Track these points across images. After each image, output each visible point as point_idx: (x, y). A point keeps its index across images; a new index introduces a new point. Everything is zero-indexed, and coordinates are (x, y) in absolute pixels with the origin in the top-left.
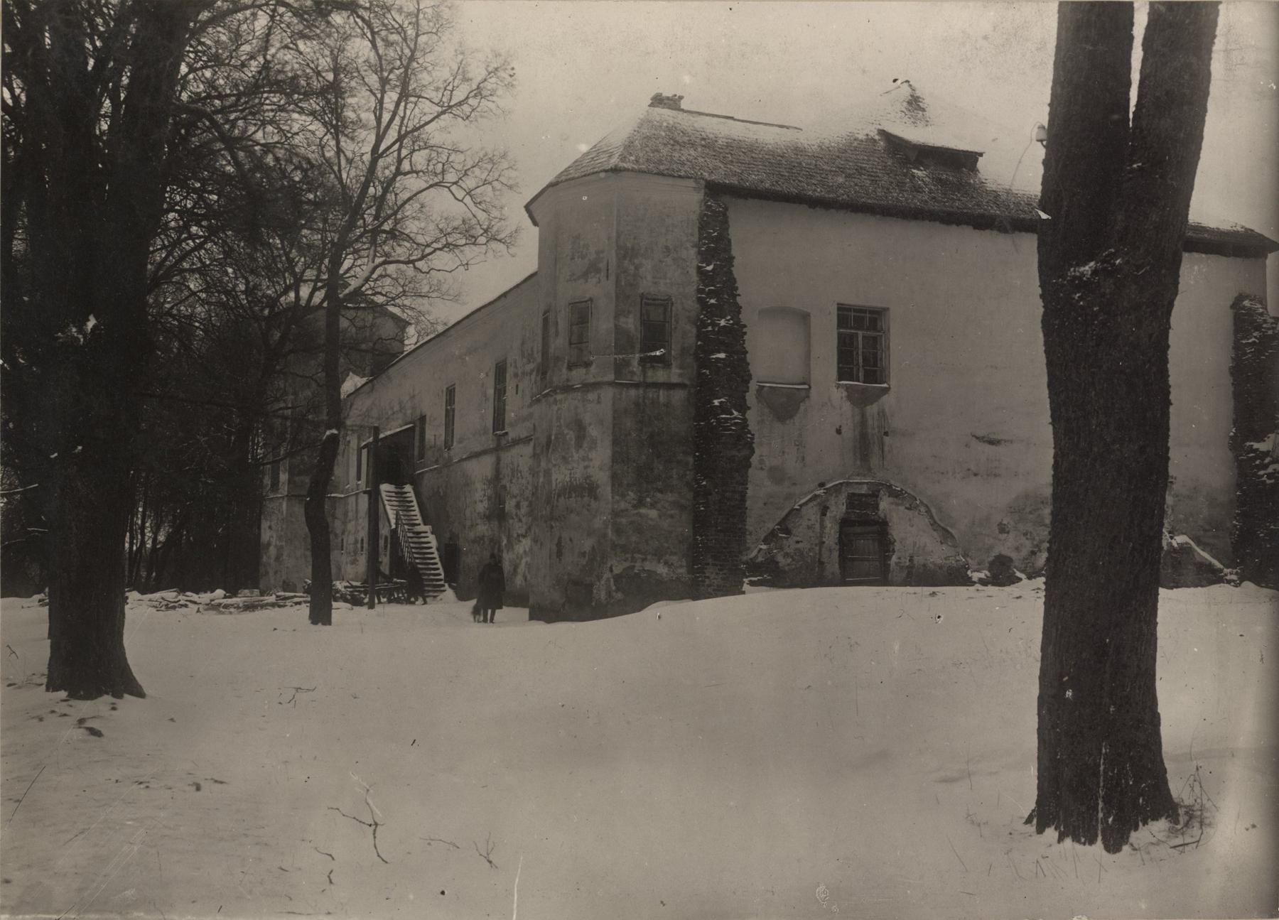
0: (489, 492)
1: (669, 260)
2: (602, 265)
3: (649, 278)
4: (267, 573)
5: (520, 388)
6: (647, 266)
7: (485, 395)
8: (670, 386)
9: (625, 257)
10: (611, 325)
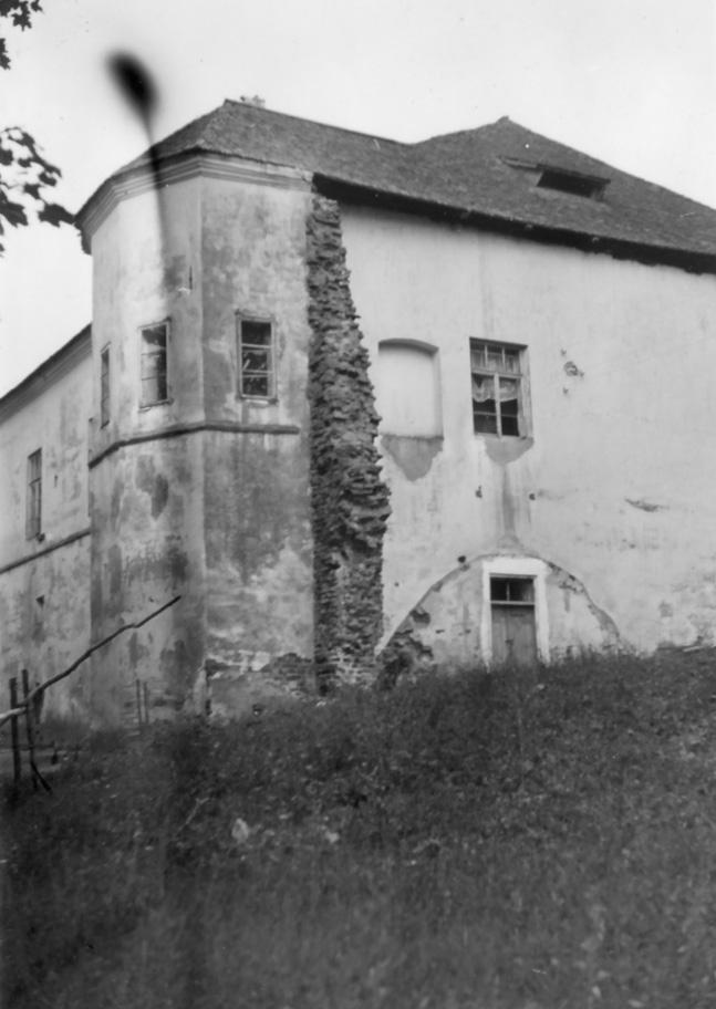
0: (21, 609)
1: (270, 271)
3: (246, 289)
5: (60, 479)
6: (243, 277)
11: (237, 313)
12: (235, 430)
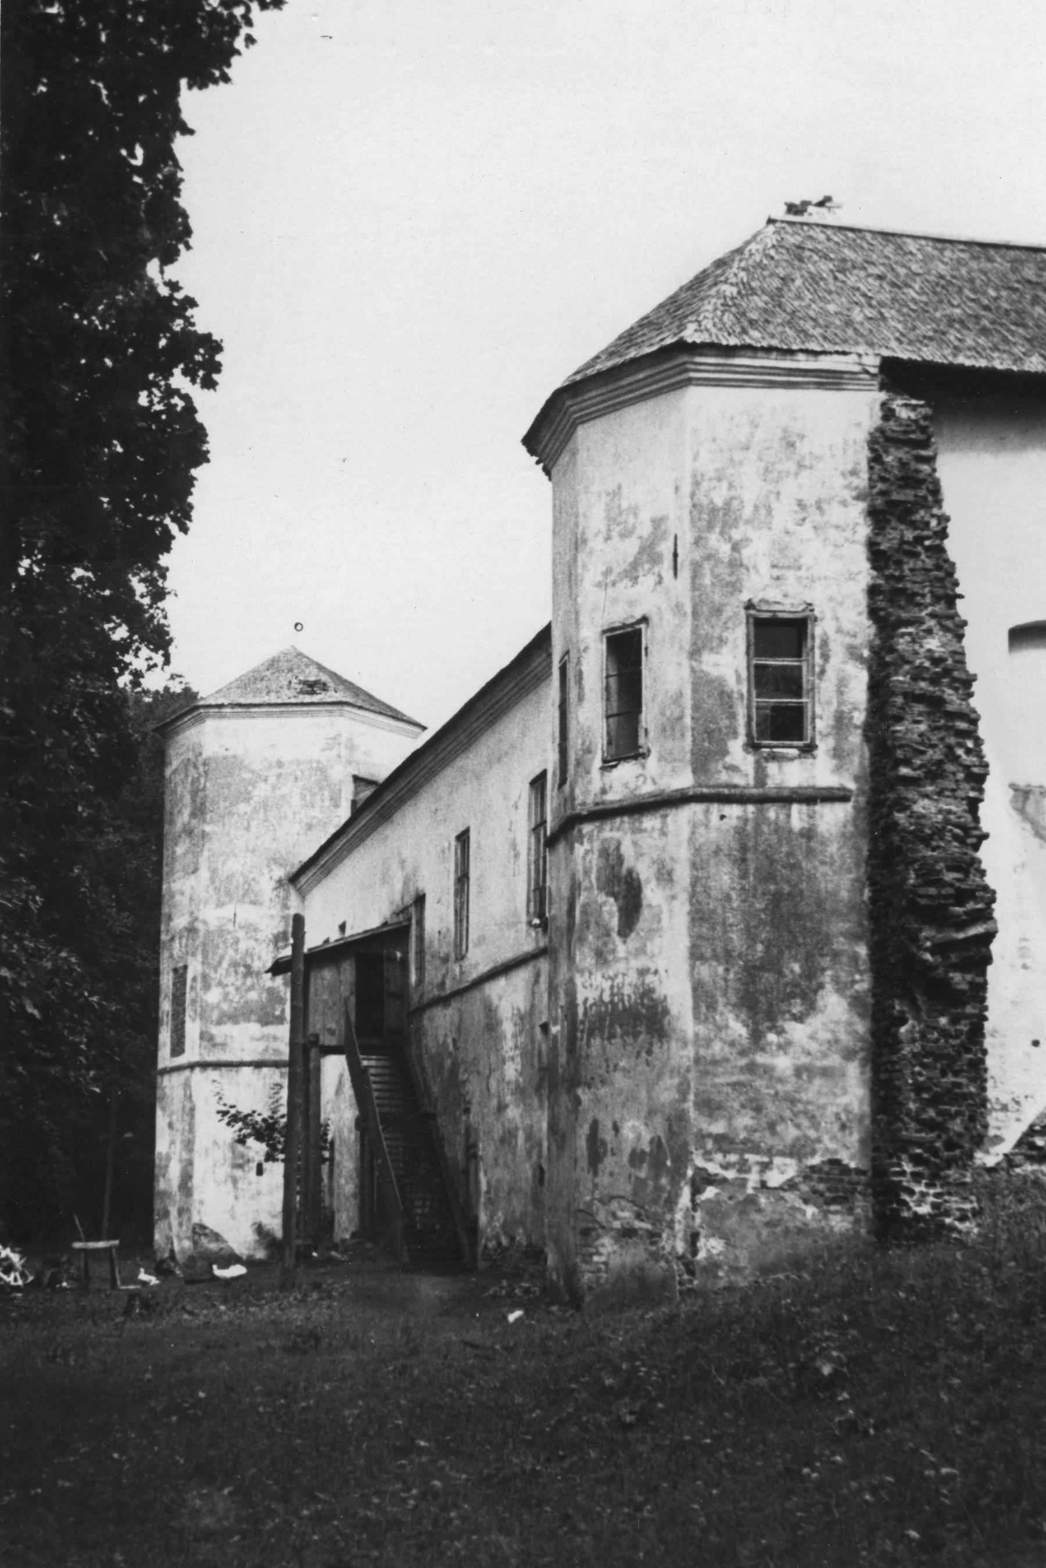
1: (806, 530)
2: (665, 548)
4: (166, 1214)
6: (758, 550)
7: (514, 846)
8: (812, 797)
9: (710, 527)
10: (686, 672)
11: (749, 606)
12: (742, 799)
